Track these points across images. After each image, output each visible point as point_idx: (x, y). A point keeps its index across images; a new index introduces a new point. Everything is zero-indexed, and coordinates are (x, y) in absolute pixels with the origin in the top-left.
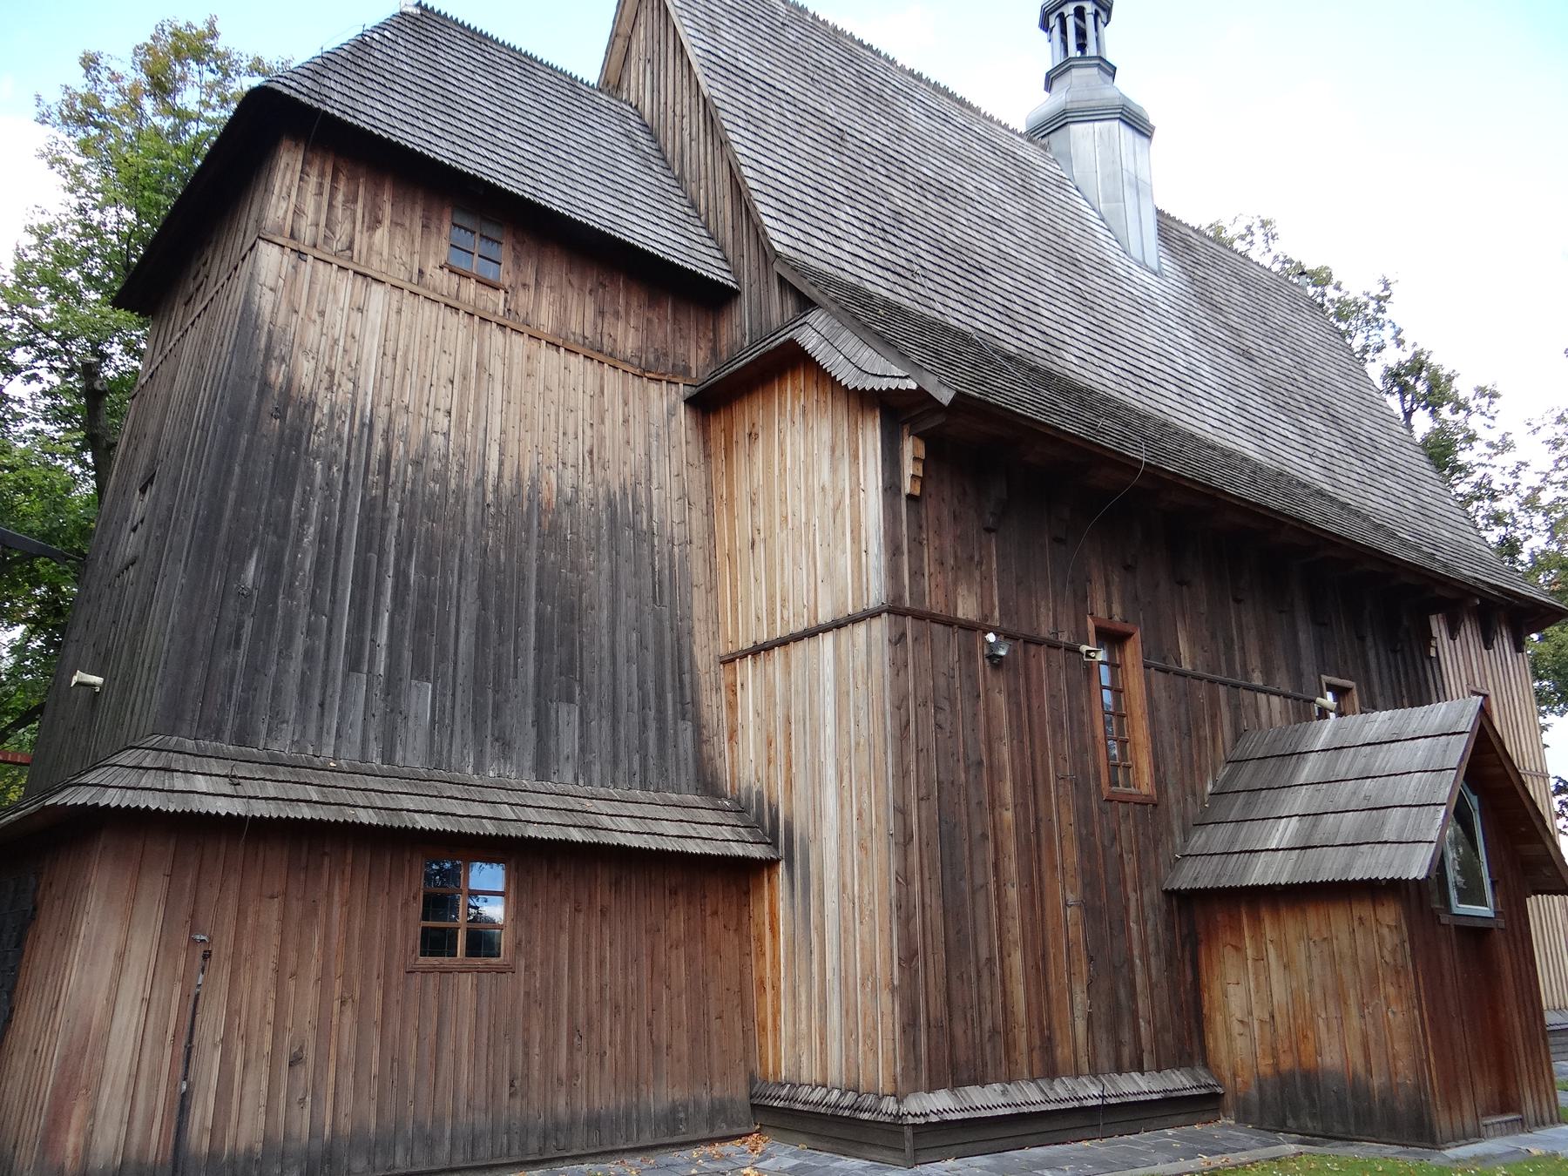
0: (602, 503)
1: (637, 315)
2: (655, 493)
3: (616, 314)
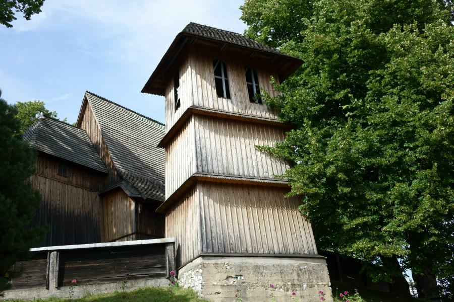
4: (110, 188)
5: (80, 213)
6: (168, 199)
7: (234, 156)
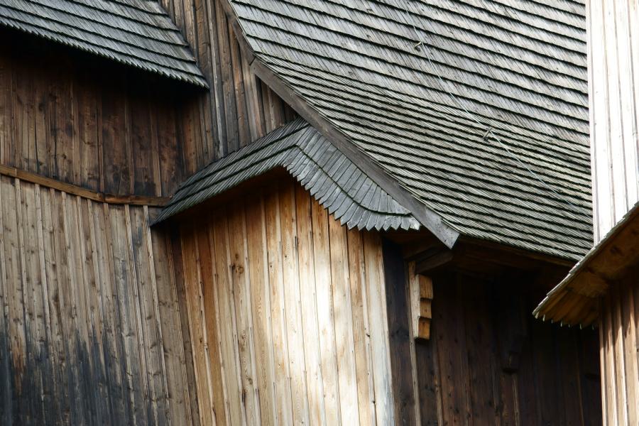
0: (73, 357)
1: (91, 128)
2: (127, 340)
3: (70, 130)
4: (223, 180)
5: (45, 342)
6: (620, 232)
7: (123, 25)
